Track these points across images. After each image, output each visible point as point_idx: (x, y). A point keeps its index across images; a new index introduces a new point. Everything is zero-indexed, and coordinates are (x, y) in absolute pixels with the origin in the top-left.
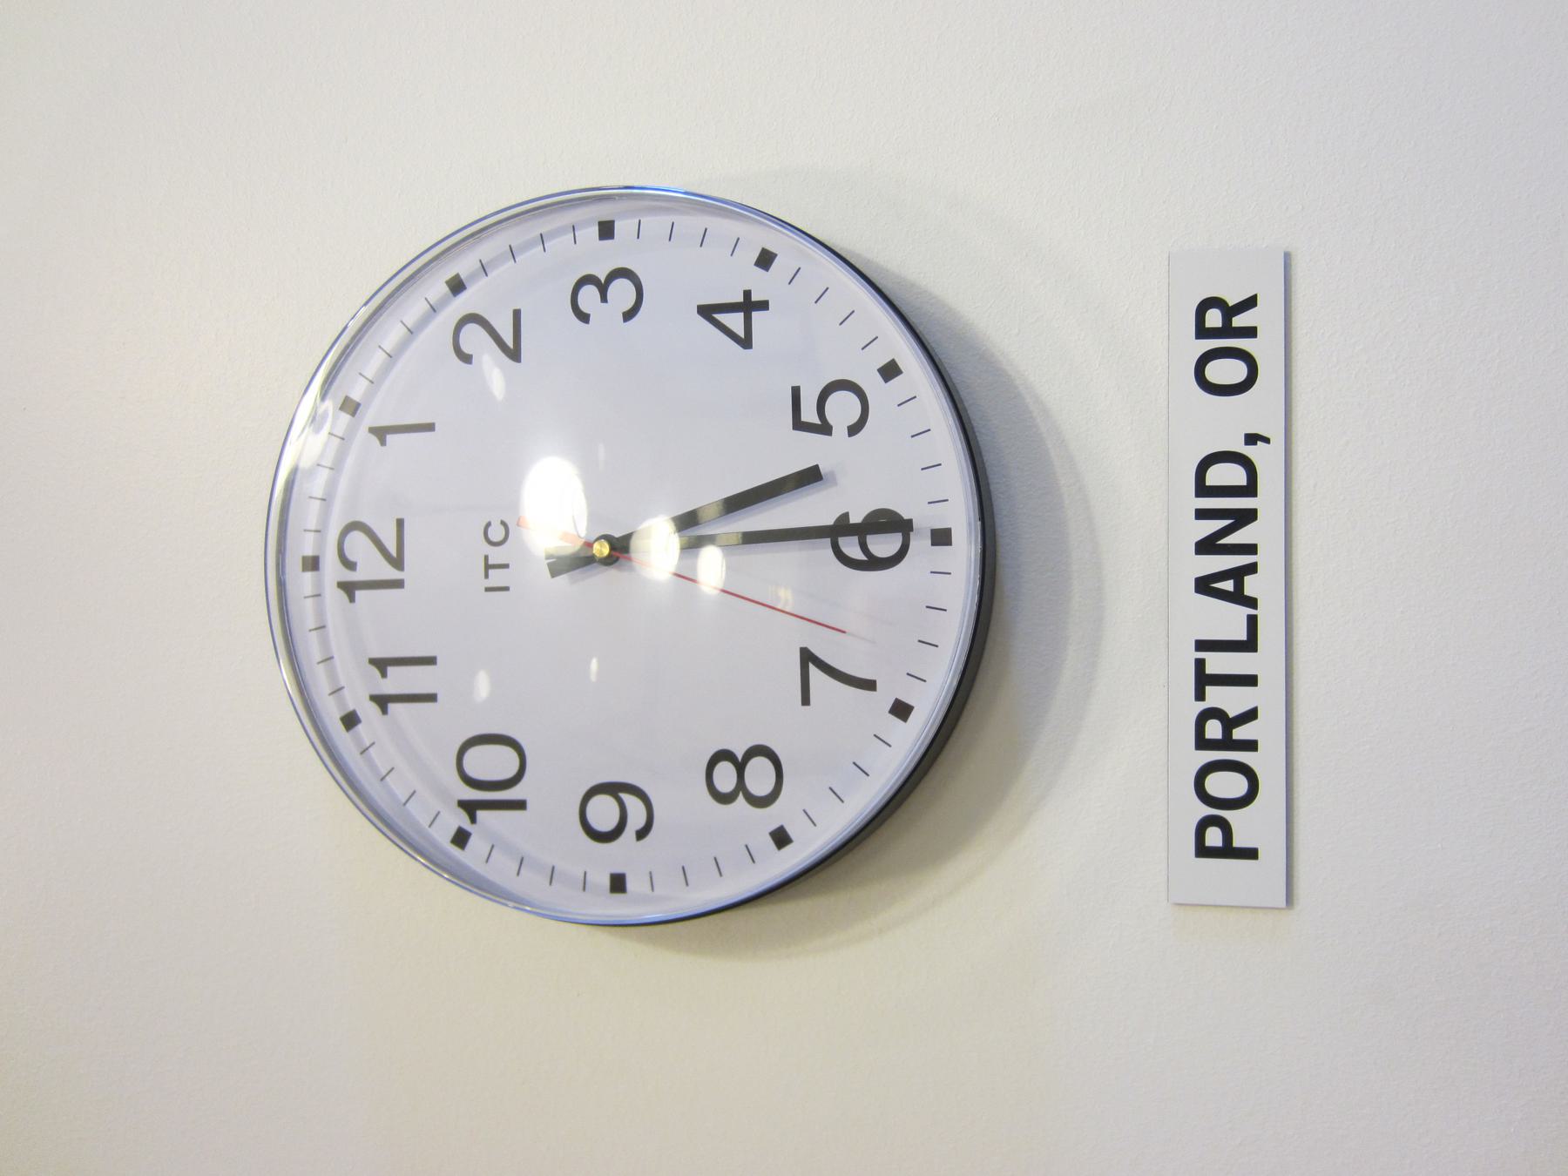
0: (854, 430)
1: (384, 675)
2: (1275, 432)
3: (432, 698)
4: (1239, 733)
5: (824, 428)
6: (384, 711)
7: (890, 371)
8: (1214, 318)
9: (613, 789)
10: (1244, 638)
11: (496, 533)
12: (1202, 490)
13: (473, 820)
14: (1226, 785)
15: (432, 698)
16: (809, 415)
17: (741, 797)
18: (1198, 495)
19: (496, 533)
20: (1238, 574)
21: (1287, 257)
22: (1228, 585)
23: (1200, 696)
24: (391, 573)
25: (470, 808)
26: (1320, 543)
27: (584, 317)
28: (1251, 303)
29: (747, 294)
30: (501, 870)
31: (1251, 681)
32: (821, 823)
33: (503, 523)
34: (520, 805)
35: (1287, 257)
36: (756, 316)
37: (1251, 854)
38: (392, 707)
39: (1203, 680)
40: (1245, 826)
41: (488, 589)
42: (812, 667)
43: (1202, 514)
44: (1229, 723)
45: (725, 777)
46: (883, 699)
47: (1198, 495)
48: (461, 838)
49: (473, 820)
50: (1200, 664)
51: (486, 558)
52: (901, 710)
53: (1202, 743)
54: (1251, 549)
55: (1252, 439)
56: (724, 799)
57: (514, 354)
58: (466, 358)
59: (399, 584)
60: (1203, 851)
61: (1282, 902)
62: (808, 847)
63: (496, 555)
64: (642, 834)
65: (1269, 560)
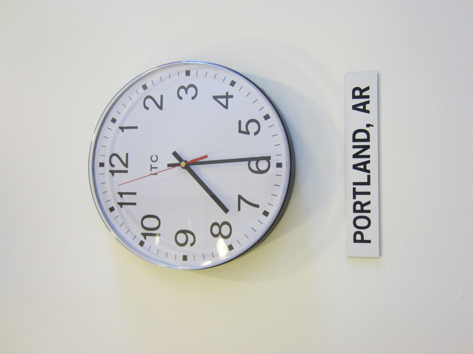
0: (256, 133)
1: (122, 197)
4: (365, 208)
5: (247, 133)
7: (267, 117)
8: (357, 93)
9: (185, 232)
11: (154, 159)
12: (355, 140)
13: (145, 239)
14: (362, 223)
15: (134, 204)
16: (243, 129)
18: (353, 141)
19: (154, 159)
20: (365, 164)
22: (361, 107)
23: (354, 198)
24: (124, 168)
25: (145, 235)
26: (387, 154)
27: (181, 98)
28: (367, 89)
29: (227, 93)
31: (368, 193)
33: (156, 156)
37: (369, 242)
39: (355, 193)
40: (367, 234)
43: (354, 147)
44: (362, 205)
45: (216, 230)
46: (261, 210)
47: (353, 141)
49: (145, 239)
50: (354, 189)
51: (151, 165)
52: (266, 214)
53: (355, 211)
54: (368, 156)
55: (368, 126)
56: (216, 236)
57: (161, 108)
58: (147, 108)
59: (126, 172)
60: (355, 241)
61: (378, 256)
63: (154, 165)
64: (192, 245)
65: (373, 159)
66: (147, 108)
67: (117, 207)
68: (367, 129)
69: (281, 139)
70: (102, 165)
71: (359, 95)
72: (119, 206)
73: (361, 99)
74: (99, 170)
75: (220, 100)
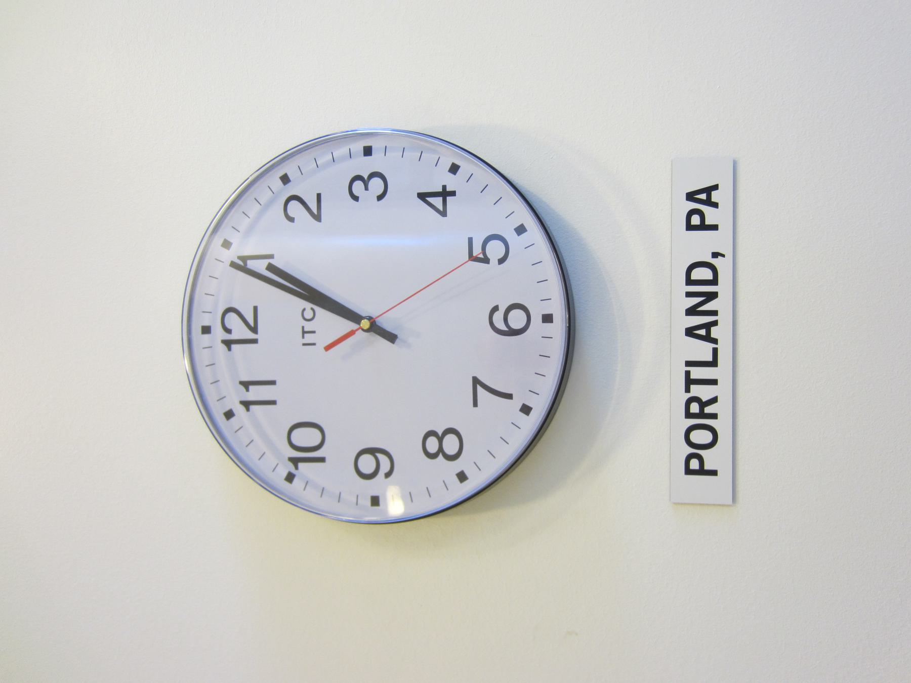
0: (501, 261)
1: (248, 390)
2: (728, 252)
3: (273, 403)
4: (707, 410)
5: (486, 260)
6: (248, 410)
7: (521, 230)
9: (372, 451)
12: (689, 282)
15: (273, 403)
16: (477, 251)
17: (441, 455)
20: (708, 326)
21: (735, 164)
22: (703, 332)
23: (688, 390)
24: (250, 335)
25: (295, 461)
26: (751, 308)
27: (356, 198)
29: (444, 187)
30: (311, 497)
31: (714, 382)
32: (483, 467)
34: (322, 460)
35: (735, 164)
36: (449, 199)
37: (714, 473)
39: (689, 381)
40: (711, 459)
41: (304, 344)
42: (479, 387)
43: (689, 295)
44: (703, 405)
45: (432, 445)
46: (516, 403)
48: (290, 478)
49: (297, 468)
50: (688, 374)
51: (303, 327)
52: (526, 410)
53: (689, 415)
54: (715, 313)
55: (715, 255)
56: (432, 456)
57: (318, 218)
58: (291, 220)
59: (255, 341)
60: (690, 227)
61: (730, 502)
63: (309, 326)
66: (291, 220)
67: (239, 410)
68: (714, 261)
70: (206, 330)
71: (699, 223)
74: (202, 340)
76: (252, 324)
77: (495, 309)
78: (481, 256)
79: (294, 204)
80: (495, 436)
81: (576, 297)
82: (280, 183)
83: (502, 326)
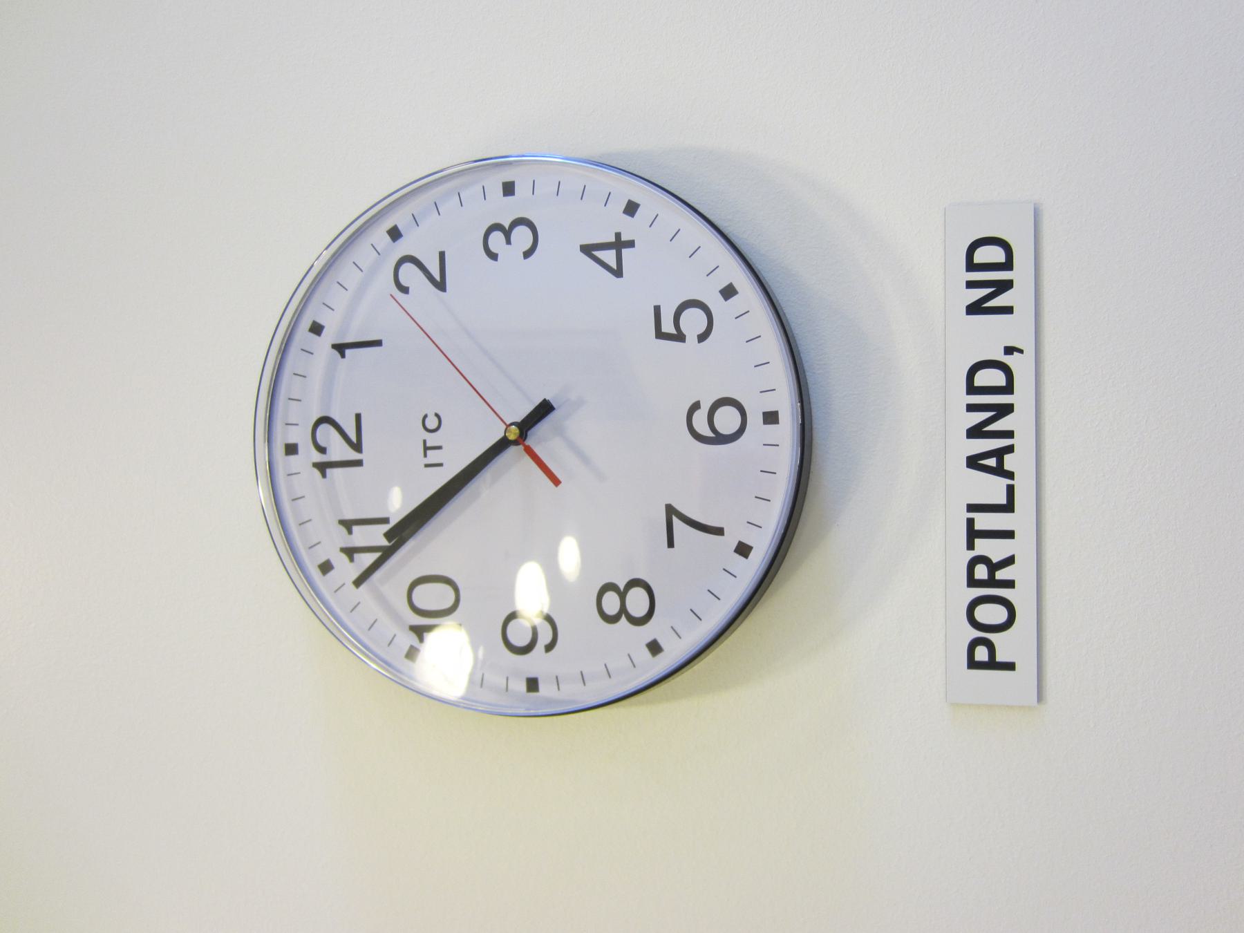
0: (702, 337)
2: (1027, 344)
4: (1001, 575)
5: (680, 337)
7: (729, 292)
10: (1004, 502)
11: (432, 423)
12: (972, 389)
14: (991, 614)
16: (668, 327)
17: (623, 618)
19: (432, 423)
20: (1000, 454)
22: (992, 462)
23: (971, 546)
24: (353, 455)
26: (1063, 426)
27: (493, 256)
29: (618, 235)
31: (1009, 535)
33: (437, 415)
36: (625, 252)
37: (1010, 666)
38: (348, 352)
39: (973, 534)
41: (427, 466)
43: (971, 408)
44: (993, 567)
46: (730, 541)
50: (970, 522)
51: (425, 442)
52: (743, 550)
53: (972, 582)
54: (1009, 434)
55: (1009, 350)
57: (441, 285)
59: (358, 463)
60: (973, 664)
62: (674, 652)
63: (432, 440)
64: (549, 647)
65: (1023, 442)
68: (1007, 360)
69: (772, 346)
72: (344, 557)
73: (990, 280)
75: (599, 254)
76: (438, 278)
77: (696, 406)
78: (673, 331)
79: (408, 268)
80: (702, 586)
81: (810, 380)
82: (388, 238)
83: (705, 431)
